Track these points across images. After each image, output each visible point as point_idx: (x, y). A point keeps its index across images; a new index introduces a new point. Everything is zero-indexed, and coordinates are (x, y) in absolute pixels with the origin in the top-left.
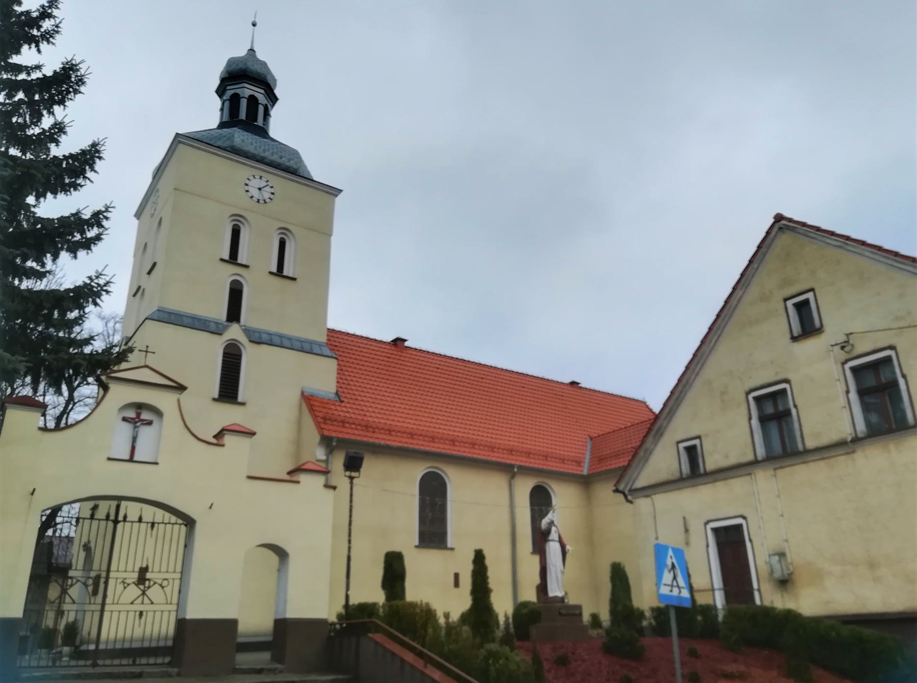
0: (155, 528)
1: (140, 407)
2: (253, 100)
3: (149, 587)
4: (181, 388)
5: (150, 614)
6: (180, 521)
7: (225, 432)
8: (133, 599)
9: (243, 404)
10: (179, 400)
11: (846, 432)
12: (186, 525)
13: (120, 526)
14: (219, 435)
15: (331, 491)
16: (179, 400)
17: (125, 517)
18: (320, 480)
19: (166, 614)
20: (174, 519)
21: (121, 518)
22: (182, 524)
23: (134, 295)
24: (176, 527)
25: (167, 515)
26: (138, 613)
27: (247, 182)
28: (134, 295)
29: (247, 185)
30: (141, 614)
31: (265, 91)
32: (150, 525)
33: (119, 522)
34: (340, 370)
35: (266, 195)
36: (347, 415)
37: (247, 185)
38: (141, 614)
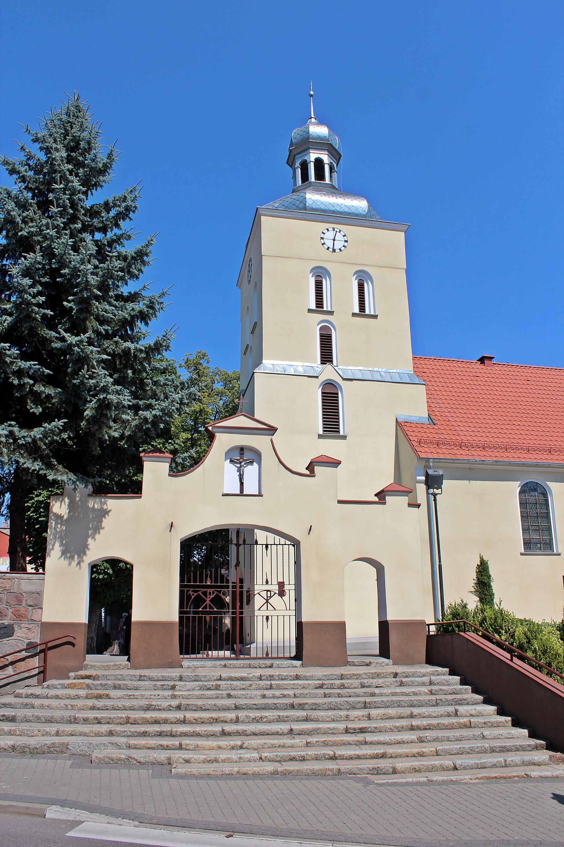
0: (269, 549)
1: (242, 449)
2: (319, 163)
3: (271, 597)
4: (272, 430)
5: (275, 618)
6: (288, 542)
7: (314, 464)
8: (48, 640)
9: (344, 437)
10: (271, 440)
11: (5, 570)
12: (293, 545)
13: (241, 548)
14: (311, 467)
15: (415, 510)
16: (271, 440)
17: (244, 541)
18: (405, 500)
19: (287, 618)
20: (283, 541)
21: (241, 542)
22: (291, 544)
23: (245, 354)
24: (286, 547)
25: (277, 538)
26: (265, 617)
27: (322, 235)
28: (245, 354)
29: (322, 238)
30: (267, 618)
31: (328, 151)
32: (264, 546)
33: (240, 545)
34: (429, 394)
35: (339, 245)
36: (441, 436)
37: (322, 238)
38: (267, 618)
